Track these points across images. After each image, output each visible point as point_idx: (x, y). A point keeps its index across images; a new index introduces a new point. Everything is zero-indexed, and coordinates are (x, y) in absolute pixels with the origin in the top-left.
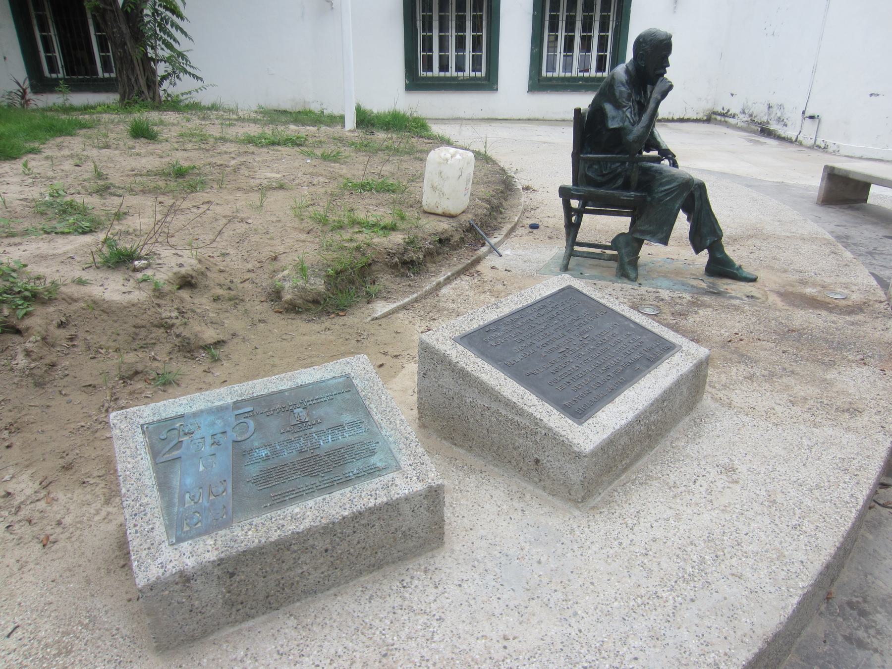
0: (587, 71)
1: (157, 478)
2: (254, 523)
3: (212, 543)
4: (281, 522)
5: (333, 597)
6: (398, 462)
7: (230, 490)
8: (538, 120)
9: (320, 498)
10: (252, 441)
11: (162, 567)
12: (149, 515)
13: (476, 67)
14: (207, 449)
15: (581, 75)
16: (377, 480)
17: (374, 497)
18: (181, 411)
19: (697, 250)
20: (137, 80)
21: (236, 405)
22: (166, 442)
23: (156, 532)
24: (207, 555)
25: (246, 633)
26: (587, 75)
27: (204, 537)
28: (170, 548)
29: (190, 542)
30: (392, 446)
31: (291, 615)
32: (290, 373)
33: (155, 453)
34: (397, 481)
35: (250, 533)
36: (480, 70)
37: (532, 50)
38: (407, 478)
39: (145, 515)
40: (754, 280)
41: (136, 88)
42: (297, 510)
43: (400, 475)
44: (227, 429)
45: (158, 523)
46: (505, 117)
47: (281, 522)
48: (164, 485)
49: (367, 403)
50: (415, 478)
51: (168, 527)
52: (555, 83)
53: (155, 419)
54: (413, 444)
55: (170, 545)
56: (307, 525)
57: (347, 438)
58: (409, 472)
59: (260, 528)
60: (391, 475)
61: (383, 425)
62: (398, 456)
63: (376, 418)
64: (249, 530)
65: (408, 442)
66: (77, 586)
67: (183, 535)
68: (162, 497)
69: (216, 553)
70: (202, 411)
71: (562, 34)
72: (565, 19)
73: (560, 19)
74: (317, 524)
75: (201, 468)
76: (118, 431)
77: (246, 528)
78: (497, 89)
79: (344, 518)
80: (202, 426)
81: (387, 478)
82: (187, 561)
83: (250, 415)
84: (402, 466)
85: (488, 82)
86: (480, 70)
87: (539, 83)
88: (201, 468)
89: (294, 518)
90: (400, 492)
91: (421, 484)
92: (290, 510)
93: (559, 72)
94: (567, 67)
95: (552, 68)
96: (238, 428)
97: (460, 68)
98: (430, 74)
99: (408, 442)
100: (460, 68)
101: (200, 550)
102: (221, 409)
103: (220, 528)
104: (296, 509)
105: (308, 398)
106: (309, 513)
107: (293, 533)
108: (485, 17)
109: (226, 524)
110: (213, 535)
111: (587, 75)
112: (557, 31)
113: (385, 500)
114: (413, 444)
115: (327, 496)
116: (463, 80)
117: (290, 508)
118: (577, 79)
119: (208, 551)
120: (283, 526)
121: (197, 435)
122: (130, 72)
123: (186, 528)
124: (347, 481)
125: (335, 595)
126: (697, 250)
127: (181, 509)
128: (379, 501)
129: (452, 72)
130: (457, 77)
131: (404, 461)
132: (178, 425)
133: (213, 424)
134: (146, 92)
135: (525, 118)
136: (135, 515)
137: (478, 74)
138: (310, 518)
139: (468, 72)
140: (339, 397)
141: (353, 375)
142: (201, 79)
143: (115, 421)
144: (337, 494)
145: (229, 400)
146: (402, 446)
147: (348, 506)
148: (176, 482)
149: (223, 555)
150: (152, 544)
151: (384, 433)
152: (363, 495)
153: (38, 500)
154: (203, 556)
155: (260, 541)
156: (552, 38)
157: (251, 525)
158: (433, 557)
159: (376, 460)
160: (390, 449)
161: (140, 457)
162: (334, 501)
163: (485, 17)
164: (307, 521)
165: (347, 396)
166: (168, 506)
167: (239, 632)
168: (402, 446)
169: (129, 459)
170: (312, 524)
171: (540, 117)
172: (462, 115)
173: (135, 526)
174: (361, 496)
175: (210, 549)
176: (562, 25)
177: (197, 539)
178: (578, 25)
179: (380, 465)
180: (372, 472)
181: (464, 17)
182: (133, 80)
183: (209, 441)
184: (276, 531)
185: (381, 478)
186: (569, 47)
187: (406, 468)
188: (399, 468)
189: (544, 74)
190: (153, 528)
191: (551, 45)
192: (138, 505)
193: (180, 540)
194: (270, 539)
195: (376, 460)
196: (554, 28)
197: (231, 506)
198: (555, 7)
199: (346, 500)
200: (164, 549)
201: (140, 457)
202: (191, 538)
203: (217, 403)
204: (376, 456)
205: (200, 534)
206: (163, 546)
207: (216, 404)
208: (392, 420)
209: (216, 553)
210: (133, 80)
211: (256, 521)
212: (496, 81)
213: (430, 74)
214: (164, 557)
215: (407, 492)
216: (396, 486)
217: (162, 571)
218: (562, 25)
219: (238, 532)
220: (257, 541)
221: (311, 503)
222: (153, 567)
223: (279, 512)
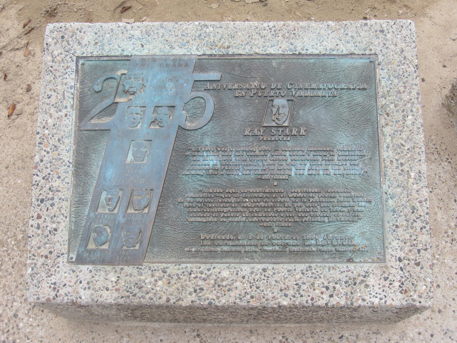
1: (77, 153)
2: (168, 271)
3: (114, 279)
4: (200, 283)
5: (248, 333)
6: (384, 248)
7: (154, 208)
9: (260, 267)
10: (204, 134)
11: (55, 289)
12: (55, 208)
14: (143, 128)
16: (343, 266)
17: (329, 293)
18: (130, 49)
21: (201, 64)
22: (102, 87)
23: (57, 238)
24: (105, 294)
25: (149, 335)
27: (108, 268)
28: (68, 267)
29: (91, 267)
30: (388, 216)
31: (198, 335)
32: (291, 24)
33: (83, 113)
34: (371, 280)
35: (160, 283)
38: (386, 279)
39: (52, 205)
42: (225, 274)
43: (379, 272)
44: (178, 103)
45: (63, 224)
47: (200, 283)
48: (81, 167)
49: (382, 122)
50: (397, 284)
51: (73, 234)
53: (95, 54)
54: (419, 224)
55: (68, 262)
56: (231, 300)
57: (331, 173)
58: (393, 271)
59: (173, 281)
60: (366, 267)
61: (389, 172)
62: (390, 237)
63: (385, 154)
64: (160, 279)
65: (413, 217)
66: (24, 185)
67: (86, 255)
68: (76, 186)
69: (116, 294)
70: (154, 59)
74: (244, 304)
75: (130, 157)
76: (50, 58)
77: (157, 274)
79: (280, 307)
80: (148, 85)
81: (357, 269)
82: (82, 292)
83: (216, 88)
84: (388, 257)
88: (130, 157)
89: (218, 285)
90: (367, 298)
91: (400, 296)
92: (217, 270)
96: (191, 104)
99: (413, 217)
101: (99, 285)
102: (178, 63)
103: (128, 263)
104: (223, 270)
106: (238, 284)
107: (210, 304)
109: (134, 260)
110: (118, 268)
113: (343, 302)
114: (419, 224)
115: (270, 266)
117: (219, 267)
119: (107, 290)
120: (202, 289)
121: (138, 100)
123: (92, 246)
124: (303, 254)
125: (251, 332)
127: (92, 215)
128: (334, 301)
131: (395, 249)
132: (119, 73)
133: (161, 88)
136: (42, 201)
138: (238, 292)
140: (346, 96)
141: (380, 58)
143: (50, 40)
144: (283, 268)
145: (195, 50)
146: (401, 221)
147: (291, 292)
148: (95, 170)
149: (121, 301)
150: (51, 253)
151: (385, 187)
152: (317, 282)
153: (18, 49)
154: (100, 293)
155: (168, 300)
157: (165, 272)
158: (377, 333)
159: (356, 232)
160: (383, 221)
161: (64, 111)
162: (276, 277)
164: (232, 294)
165: (359, 97)
166: (79, 202)
167: (144, 329)
168: (401, 221)
169: (53, 110)
170: (238, 301)
173: (39, 217)
174: (313, 284)
175: (110, 287)
177: (99, 267)
179: (357, 241)
180: (343, 252)
183: (150, 115)
184: (190, 294)
185: (351, 266)
187: (392, 262)
188: (382, 259)
190: (56, 230)
192: (48, 186)
193: (80, 260)
194: (180, 302)
195: (356, 232)
197: (148, 234)
199: (291, 282)
200: (61, 265)
201: (64, 111)
202: (93, 263)
203: (178, 51)
204: (359, 224)
205: (103, 262)
206: (60, 259)
207: (175, 52)
208: (406, 168)
209: (116, 294)
211: (172, 269)
214: (58, 276)
215: (376, 301)
216: (367, 286)
217: (53, 294)
219: (146, 278)
220: (164, 298)
221: (246, 269)
222: (45, 285)
223: (203, 266)
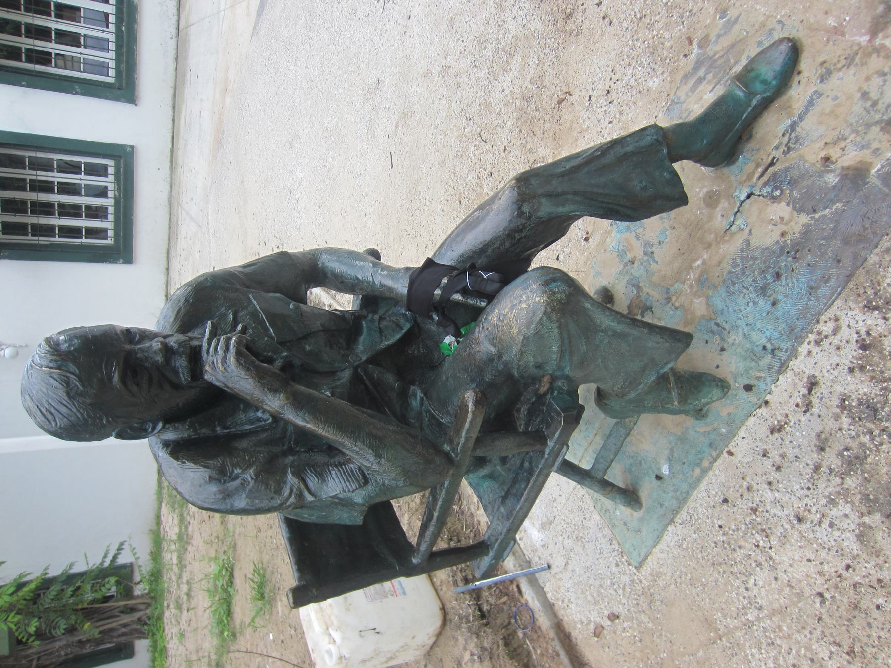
0: (107, 15)
8: (174, 96)
13: (101, 171)
15: (112, 28)
19: (676, 198)
20: (125, 626)
26: (112, 19)
36: (106, 167)
37: (77, 93)
40: (795, 50)
41: (134, 626)
46: (170, 139)
52: (123, 66)
71: (53, 47)
72: (34, 172)
73: (34, 177)
78: (132, 147)
85: (122, 157)
86: (106, 167)
87: (123, 88)
93: (109, 57)
94: (101, 45)
95: (102, 68)
97: (102, 193)
98: (111, 210)
100: (102, 193)
105: (519, 500)
108: (32, 154)
111: (112, 19)
112: (53, 182)
116: (119, 189)
118: (119, 33)
122: (115, 634)
126: (676, 198)
129: (108, 202)
130: (115, 198)
134: (137, 615)
135: (171, 113)
137: (111, 170)
139: (108, 182)
142: (122, 544)
156: (61, 62)
163: (32, 154)
171: (171, 91)
172: (165, 195)
176: (40, 45)
178: (44, 220)
181: (34, 226)
182: (124, 630)
186: (73, 39)
189: (111, 80)
191: (69, 64)
196: (44, 58)
198: (14, 53)
210: (124, 630)
212: (122, 147)
213: (111, 210)
218: (40, 45)
